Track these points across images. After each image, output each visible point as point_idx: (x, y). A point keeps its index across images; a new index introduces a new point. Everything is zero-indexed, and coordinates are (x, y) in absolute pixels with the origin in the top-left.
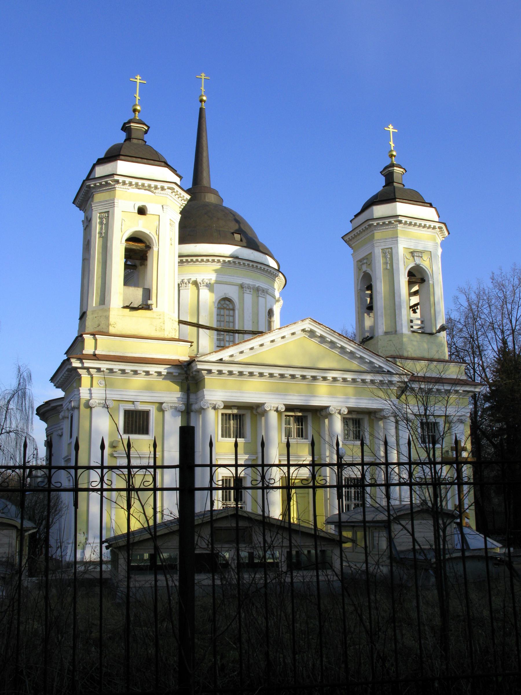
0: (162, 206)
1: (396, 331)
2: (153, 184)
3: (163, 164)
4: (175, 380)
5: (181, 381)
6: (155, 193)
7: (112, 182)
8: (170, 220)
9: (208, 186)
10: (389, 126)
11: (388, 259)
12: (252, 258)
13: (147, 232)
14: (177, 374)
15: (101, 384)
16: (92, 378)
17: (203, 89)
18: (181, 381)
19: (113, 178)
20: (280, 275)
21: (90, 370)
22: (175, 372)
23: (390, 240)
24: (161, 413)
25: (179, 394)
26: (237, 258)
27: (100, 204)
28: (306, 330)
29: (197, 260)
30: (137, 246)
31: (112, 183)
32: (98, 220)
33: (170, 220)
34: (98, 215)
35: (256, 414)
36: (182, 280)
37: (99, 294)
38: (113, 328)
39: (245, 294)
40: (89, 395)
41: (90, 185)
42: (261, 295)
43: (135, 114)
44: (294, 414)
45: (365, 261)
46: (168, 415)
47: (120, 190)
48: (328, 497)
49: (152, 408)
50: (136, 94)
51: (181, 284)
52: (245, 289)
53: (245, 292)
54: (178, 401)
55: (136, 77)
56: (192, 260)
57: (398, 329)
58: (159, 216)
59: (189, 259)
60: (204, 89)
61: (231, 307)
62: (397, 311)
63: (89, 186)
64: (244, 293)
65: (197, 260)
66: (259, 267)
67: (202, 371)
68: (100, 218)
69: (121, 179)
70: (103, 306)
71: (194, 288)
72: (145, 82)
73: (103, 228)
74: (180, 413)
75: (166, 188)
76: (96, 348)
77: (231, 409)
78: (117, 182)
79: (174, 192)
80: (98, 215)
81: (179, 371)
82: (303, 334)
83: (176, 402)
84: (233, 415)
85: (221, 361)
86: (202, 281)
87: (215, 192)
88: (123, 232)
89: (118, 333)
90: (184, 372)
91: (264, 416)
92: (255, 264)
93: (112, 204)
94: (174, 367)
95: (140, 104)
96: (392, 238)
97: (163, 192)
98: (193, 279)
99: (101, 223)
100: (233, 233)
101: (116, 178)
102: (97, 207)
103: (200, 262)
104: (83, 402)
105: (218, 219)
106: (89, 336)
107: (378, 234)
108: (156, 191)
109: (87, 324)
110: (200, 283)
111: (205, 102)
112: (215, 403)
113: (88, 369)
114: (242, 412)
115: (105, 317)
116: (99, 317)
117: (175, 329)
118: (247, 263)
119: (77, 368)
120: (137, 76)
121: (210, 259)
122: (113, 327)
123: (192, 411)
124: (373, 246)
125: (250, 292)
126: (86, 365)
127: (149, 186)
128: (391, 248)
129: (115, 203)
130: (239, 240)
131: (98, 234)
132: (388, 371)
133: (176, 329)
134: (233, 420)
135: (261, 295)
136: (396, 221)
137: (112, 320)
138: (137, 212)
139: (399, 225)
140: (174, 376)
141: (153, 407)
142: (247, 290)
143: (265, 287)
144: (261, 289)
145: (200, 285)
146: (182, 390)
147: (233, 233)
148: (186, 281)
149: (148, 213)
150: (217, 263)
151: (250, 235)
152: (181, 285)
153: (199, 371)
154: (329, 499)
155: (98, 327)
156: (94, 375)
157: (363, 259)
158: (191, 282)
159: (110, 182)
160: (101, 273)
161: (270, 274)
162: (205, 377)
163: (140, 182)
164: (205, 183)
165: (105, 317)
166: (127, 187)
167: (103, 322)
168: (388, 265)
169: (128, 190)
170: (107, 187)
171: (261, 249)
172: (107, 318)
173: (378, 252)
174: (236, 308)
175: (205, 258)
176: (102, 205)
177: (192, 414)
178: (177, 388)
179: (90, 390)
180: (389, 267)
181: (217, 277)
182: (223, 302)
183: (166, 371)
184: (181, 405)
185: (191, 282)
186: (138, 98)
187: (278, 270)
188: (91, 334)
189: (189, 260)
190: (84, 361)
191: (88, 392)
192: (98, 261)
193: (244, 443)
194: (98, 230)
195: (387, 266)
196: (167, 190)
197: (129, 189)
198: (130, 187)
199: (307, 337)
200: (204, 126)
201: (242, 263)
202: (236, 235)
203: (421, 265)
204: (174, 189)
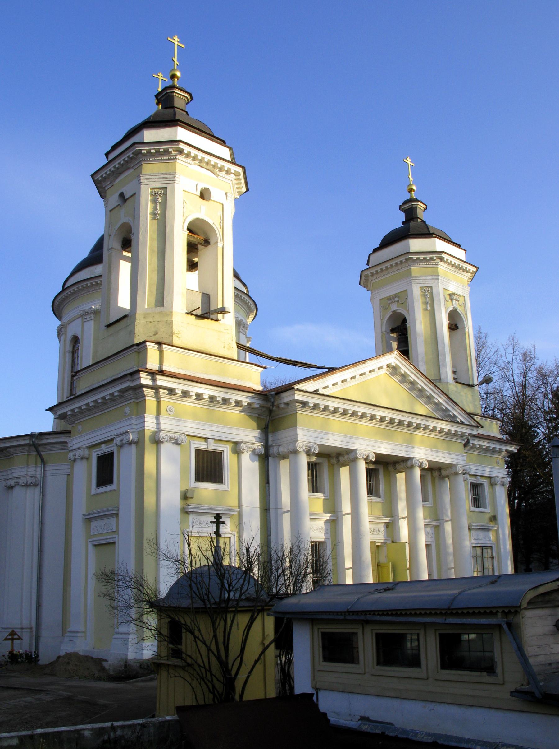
0: (226, 193)
1: (440, 379)
4: (253, 415)
6: (218, 176)
10: (408, 159)
11: (427, 298)
13: (211, 222)
14: (258, 406)
15: (171, 411)
18: (257, 415)
22: (257, 402)
23: (431, 278)
34: (150, 190)
37: (155, 292)
38: (177, 338)
40: (155, 426)
41: (141, 150)
45: (396, 299)
46: (246, 457)
47: (181, 163)
48: (408, 566)
50: (174, 58)
57: (442, 377)
62: (440, 357)
69: (187, 149)
72: (184, 46)
73: (158, 208)
74: (257, 458)
78: (181, 152)
80: (150, 190)
85: (316, 392)
88: (184, 218)
91: (145, 396)
94: (256, 396)
96: (432, 276)
104: (147, 434)
106: (153, 344)
107: (415, 270)
109: (136, 330)
124: (410, 283)
126: (159, 383)
128: (431, 287)
129: (176, 179)
131: (150, 214)
132: (461, 421)
136: (438, 258)
137: (175, 328)
139: (440, 263)
141: (227, 448)
154: (408, 569)
157: (395, 296)
160: (156, 266)
166: (189, 160)
167: (162, 330)
168: (428, 305)
173: (416, 291)
176: (156, 178)
180: (429, 308)
191: (155, 421)
193: (324, 499)
194: (149, 210)
195: (427, 306)
197: (190, 164)
198: (192, 162)
203: (458, 310)
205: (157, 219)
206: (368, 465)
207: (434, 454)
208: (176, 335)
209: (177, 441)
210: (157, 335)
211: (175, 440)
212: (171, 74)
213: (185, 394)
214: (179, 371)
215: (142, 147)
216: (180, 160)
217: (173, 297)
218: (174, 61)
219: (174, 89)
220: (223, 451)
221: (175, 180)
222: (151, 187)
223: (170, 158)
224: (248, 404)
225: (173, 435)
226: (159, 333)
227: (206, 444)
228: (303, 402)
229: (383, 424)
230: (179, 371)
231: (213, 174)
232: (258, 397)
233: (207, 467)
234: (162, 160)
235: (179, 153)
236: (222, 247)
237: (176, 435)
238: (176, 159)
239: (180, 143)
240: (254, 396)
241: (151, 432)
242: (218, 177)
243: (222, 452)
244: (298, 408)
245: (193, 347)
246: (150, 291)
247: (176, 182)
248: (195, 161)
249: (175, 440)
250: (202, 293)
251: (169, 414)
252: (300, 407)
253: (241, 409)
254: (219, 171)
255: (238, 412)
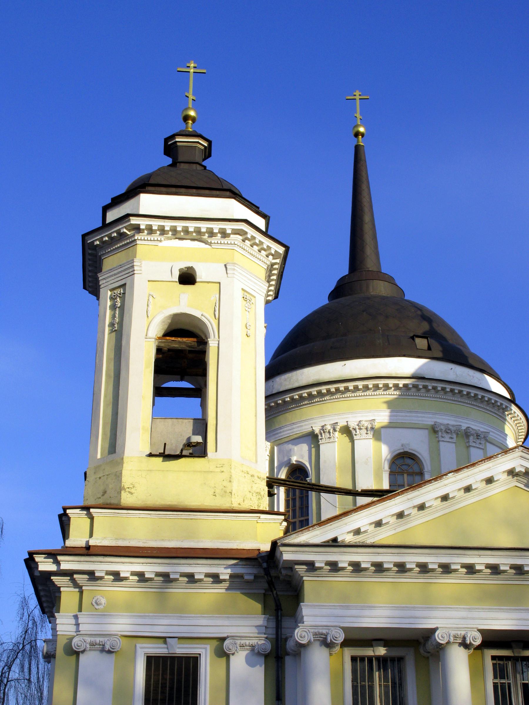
0: (225, 265)
2: (204, 226)
3: (228, 193)
5: (263, 592)
6: (210, 244)
7: (129, 231)
8: (243, 290)
9: (375, 269)
12: (451, 377)
13: (197, 314)
14: (252, 578)
16: (81, 592)
17: (358, 115)
19: (129, 223)
20: (514, 408)
21: (75, 576)
24: (224, 659)
25: (260, 620)
26: (423, 378)
27: (111, 274)
28: (517, 470)
29: (347, 389)
30: (180, 342)
31: (129, 233)
32: (109, 303)
33: (243, 290)
34: (109, 293)
35: (426, 654)
36: (323, 426)
38: (129, 495)
39: (441, 443)
40: (73, 628)
41: (93, 242)
42: (474, 444)
43: (187, 123)
44: (512, 655)
49: (203, 651)
50: (188, 92)
51: (321, 434)
52: (440, 434)
53: (441, 439)
54: (258, 633)
55: (188, 65)
56: (338, 390)
58: (219, 283)
59: (332, 388)
60: (361, 114)
61: (416, 469)
63: (92, 246)
64: (439, 441)
65: (347, 389)
66: (473, 395)
67: (296, 567)
68: (111, 298)
69: (143, 223)
70: (113, 455)
71: (345, 439)
74: (262, 660)
75: (229, 231)
76: (91, 535)
77: (371, 646)
78: (137, 229)
79: (247, 239)
80: (109, 293)
81: (254, 571)
82: (513, 482)
83: (256, 635)
84: (378, 658)
86: (358, 425)
87: (390, 280)
89: (139, 504)
90: (262, 573)
91: (60, 587)
92: (457, 388)
93: (131, 270)
94: (244, 563)
95: (194, 108)
97: (225, 241)
98: (342, 423)
99: (113, 307)
100: (413, 338)
101: (134, 221)
102: (107, 280)
103: (353, 392)
105: (387, 317)
106: (78, 511)
108: (213, 240)
110: (355, 429)
111: (363, 135)
112: (324, 631)
113: (70, 574)
114: (396, 652)
115: (116, 475)
116: (106, 477)
117: (258, 493)
118: (440, 386)
119: (50, 574)
120: (189, 62)
121: (370, 383)
122: (130, 492)
123: (288, 654)
125: (452, 438)
126: (64, 566)
127: (198, 231)
129: (135, 268)
130: (426, 347)
131: (109, 326)
133: (262, 493)
134: (379, 670)
135: (474, 444)
137: (127, 479)
138: (177, 280)
140: (248, 582)
142: (445, 435)
143: (482, 430)
144: (473, 432)
145: (354, 432)
146: (265, 611)
147: (413, 338)
148: (329, 427)
149: (198, 280)
150: (384, 390)
151: (451, 341)
152: (322, 436)
153: (291, 565)
155: (103, 495)
156: (84, 588)
158: (338, 428)
159: (125, 230)
161: (496, 408)
162: (305, 578)
163: (180, 225)
164: (370, 264)
165: (116, 475)
166: (156, 236)
169: (160, 244)
170: (121, 242)
171: (471, 361)
172: (118, 477)
174: (426, 469)
175: (360, 384)
176: (115, 275)
177: (288, 661)
178: (258, 607)
179: (76, 617)
181: (390, 416)
182: (400, 462)
183: (229, 571)
184: (263, 642)
185: (338, 428)
186: (191, 97)
187: (513, 401)
188: (83, 508)
189: (333, 390)
190: (60, 558)
191: (73, 621)
192: (107, 375)
194: (107, 322)
196: (232, 236)
197: (161, 241)
199: (522, 486)
200: (364, 174)
201: (430, 388)
202: (418, 340)
204: (246, 233)
205: (115, 331)
206: (513, 652)
207: (97, 620)
208: (127, 490)
209: (103, 648)
210: (106, 495)
211: (251, 648)
212: (183, 115)
213: (446, 569)
214: (117, 542)
215: (93, 238)
216: (141, 240)
217: (125, 437)
218: (188, 97)
219: (175, 138)
220: (200, 654)
221: (134, 270)
222: (110, 288)
223: (128, 241)
224: (230, 576)
225: (98, 640)
226: (108, 492)
227: (166, 646)
228: (306, 562)
229: (454, 575)
230: (117, 542)
231: (204, 244)
232: (248, 563)
233: (179, 681)
234: (121, 247)
235: (136, 231)
236: (217, 345)
237: (102, 639)
238: (135, 240)
239: (131, 218)
240: (240, 563)
241: (67, 639)
242: (211, 246)
243: (198, 656)
244: (303, 572)
245: (157, 503)
246: (104, 433)
247: (135, 272)
248: (165, 235)
249: (251, 648)
250: (194, 419)
251: (96, 609)
252: (306, 571)
253: (228, 585)
254: (209, 237)
255: (223, 591)
